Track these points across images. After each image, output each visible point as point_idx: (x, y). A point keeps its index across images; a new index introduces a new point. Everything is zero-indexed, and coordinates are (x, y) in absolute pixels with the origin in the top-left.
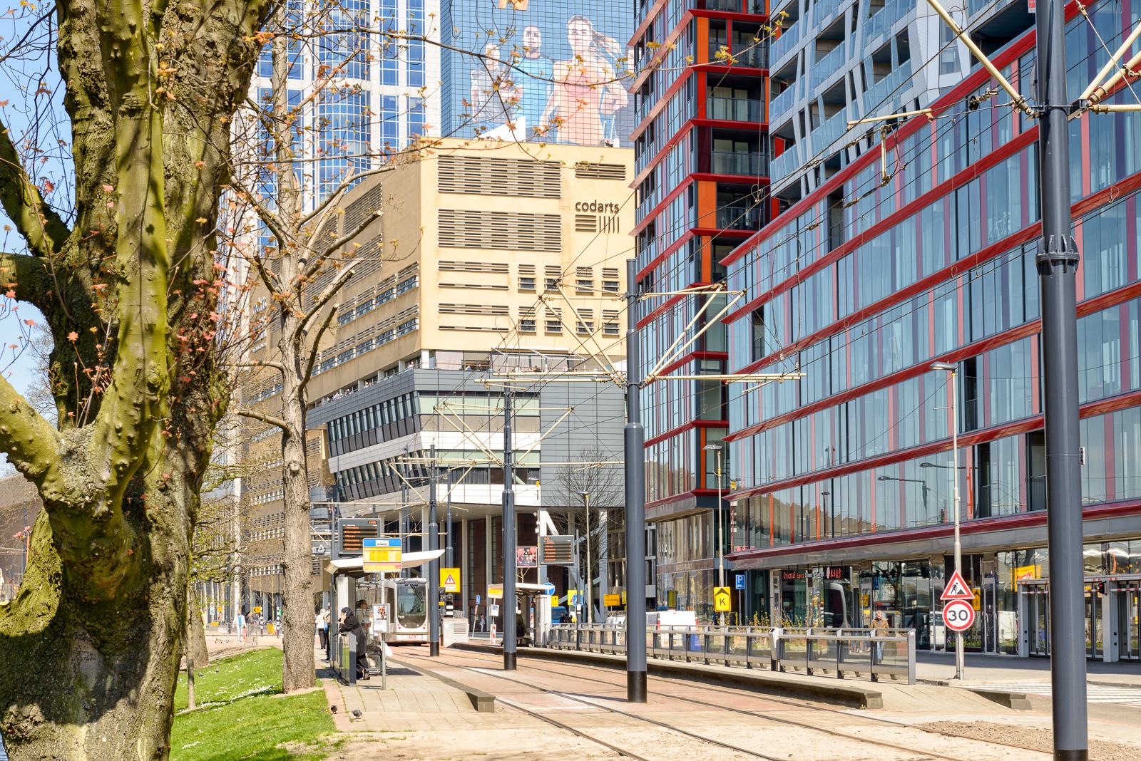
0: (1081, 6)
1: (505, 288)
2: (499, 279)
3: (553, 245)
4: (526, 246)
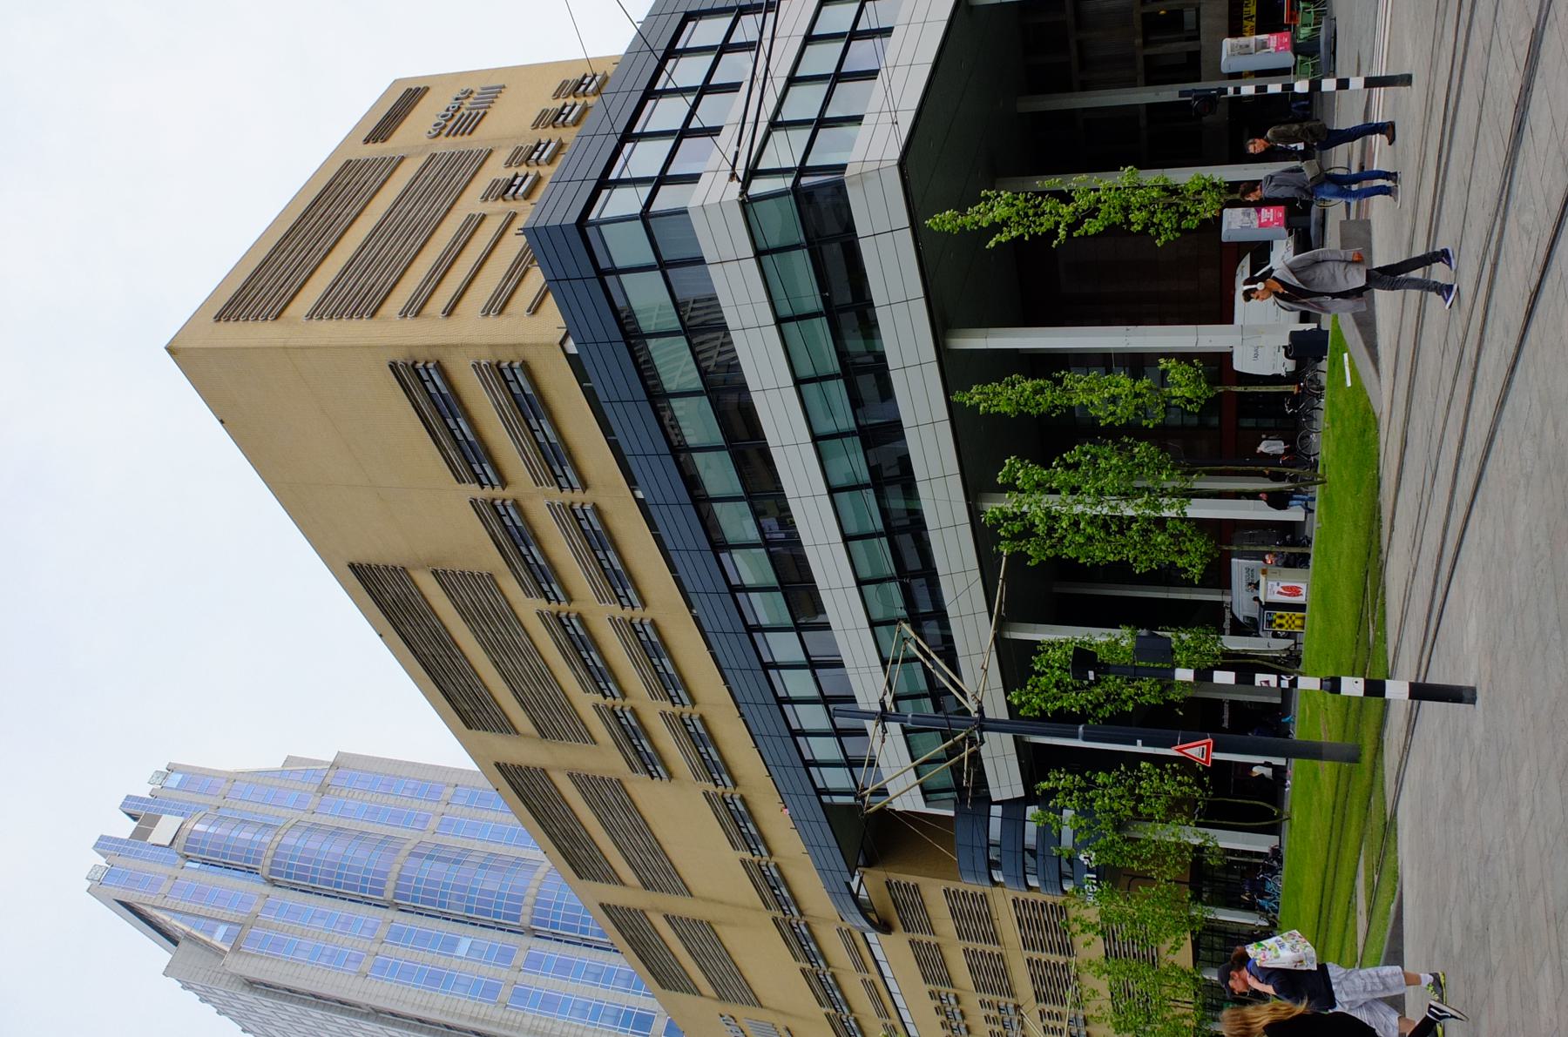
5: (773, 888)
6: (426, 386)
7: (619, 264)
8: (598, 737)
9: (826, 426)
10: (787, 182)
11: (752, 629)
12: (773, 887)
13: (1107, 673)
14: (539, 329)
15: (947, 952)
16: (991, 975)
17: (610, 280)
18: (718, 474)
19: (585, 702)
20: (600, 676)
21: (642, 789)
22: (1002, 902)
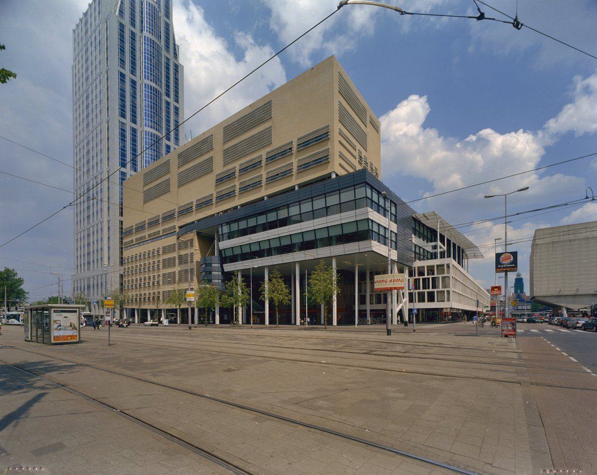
6: (322, 137)
7: (314, 202)
9: (271, 242)
10: (370, 228)
11: (288, 206)
13: (399, 289)
14: (337, 168)
16: (169, 263)
17: (338, 192)
18: (243, 225)
19: (237, 165)
20: (244, 170)
21: (211, 179)
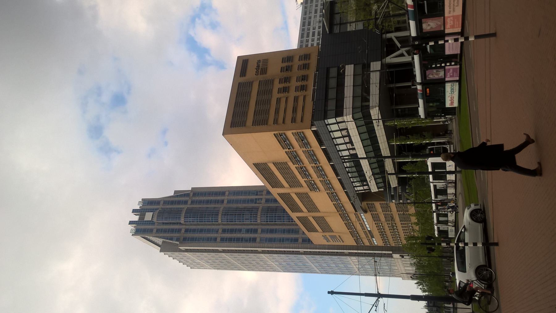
0: (419, 87)
1: (305, 97)
2: (283, 100)
3: (272, 82)
4: (271, 92)
5: (302, 141)
8: (303, 185)
12: (340, 208)
15: (380, 215)
19: (302, 181)
21: (313, 195)
22: (393, 205)
